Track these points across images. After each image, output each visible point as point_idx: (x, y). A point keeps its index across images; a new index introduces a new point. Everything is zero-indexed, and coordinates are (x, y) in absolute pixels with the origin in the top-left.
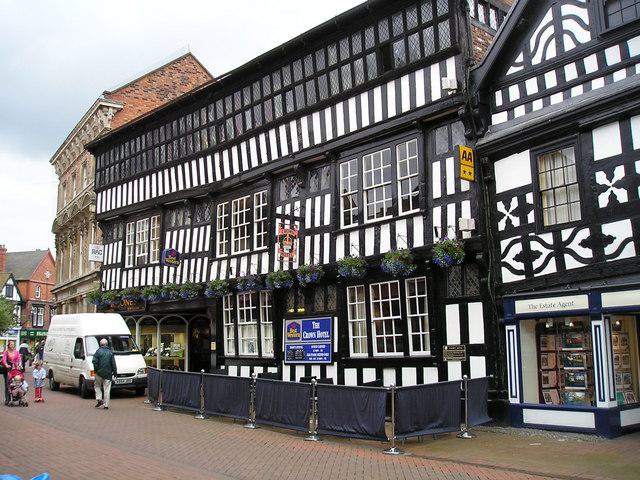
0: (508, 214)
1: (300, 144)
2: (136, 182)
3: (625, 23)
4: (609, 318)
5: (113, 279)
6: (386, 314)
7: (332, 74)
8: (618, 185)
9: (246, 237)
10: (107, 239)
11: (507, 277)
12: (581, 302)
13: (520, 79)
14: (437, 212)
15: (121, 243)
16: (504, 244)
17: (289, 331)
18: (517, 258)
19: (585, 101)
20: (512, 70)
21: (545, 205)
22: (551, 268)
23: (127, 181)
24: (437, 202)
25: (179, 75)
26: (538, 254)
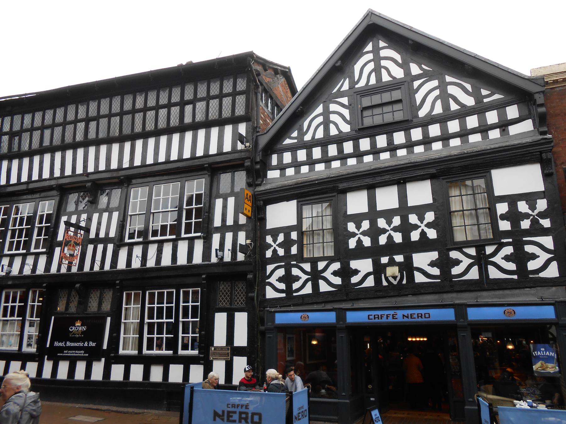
0: (274, 246)
6: (160, 316)
7: (125, 117)
8: (364, 234)
11: (270, 294)
13: (293, 149)
14: (216, 238)
16: (270, 268)
18: (280, 280)
19: (324, 176)
20: (288, 141)
21: (305, 242)
22: (308, 290)
24: (217, 230)
26: (297, 278)
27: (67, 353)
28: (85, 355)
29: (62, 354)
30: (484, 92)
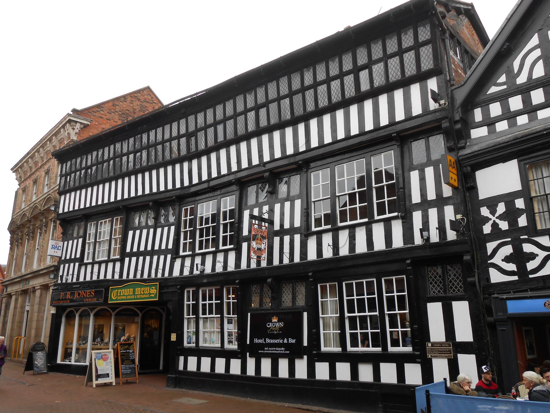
1: (209, 173)
5: (71, 272)
9: (211, 237)
10: (66, 236)
11: (496, 277)
13: (502, 97)
15: (81, 240)
16: (491, 246)
20: (493, 90)
23: (92, 185)
24: (417, 207)
25: (139, 103)
27: (268, 350)
28: (286, 352)
29: (263, 352)
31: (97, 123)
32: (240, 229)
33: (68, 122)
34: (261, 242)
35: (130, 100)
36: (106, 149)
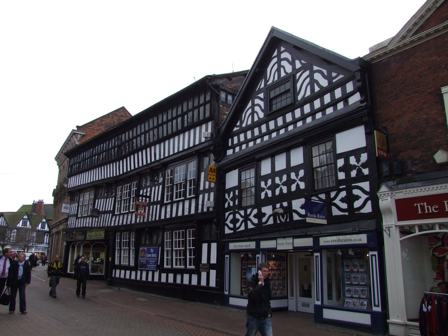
2: (144, 151)
3: (282, 107)
4: (265, 254)
6: (179, 247)
7: (135, 135)
10: (72, 201)
11: (227, 231)
12: (252, 245)
16: (227, 214)
17: (141, 253)
20: (235, 129)
22: (242, 228)
30: (334, 74)
31: (91, 133)
32: (198, 185)
33: (73, 134)
34: (142, 208)
35: (112, 116)
36: (127, 133)
